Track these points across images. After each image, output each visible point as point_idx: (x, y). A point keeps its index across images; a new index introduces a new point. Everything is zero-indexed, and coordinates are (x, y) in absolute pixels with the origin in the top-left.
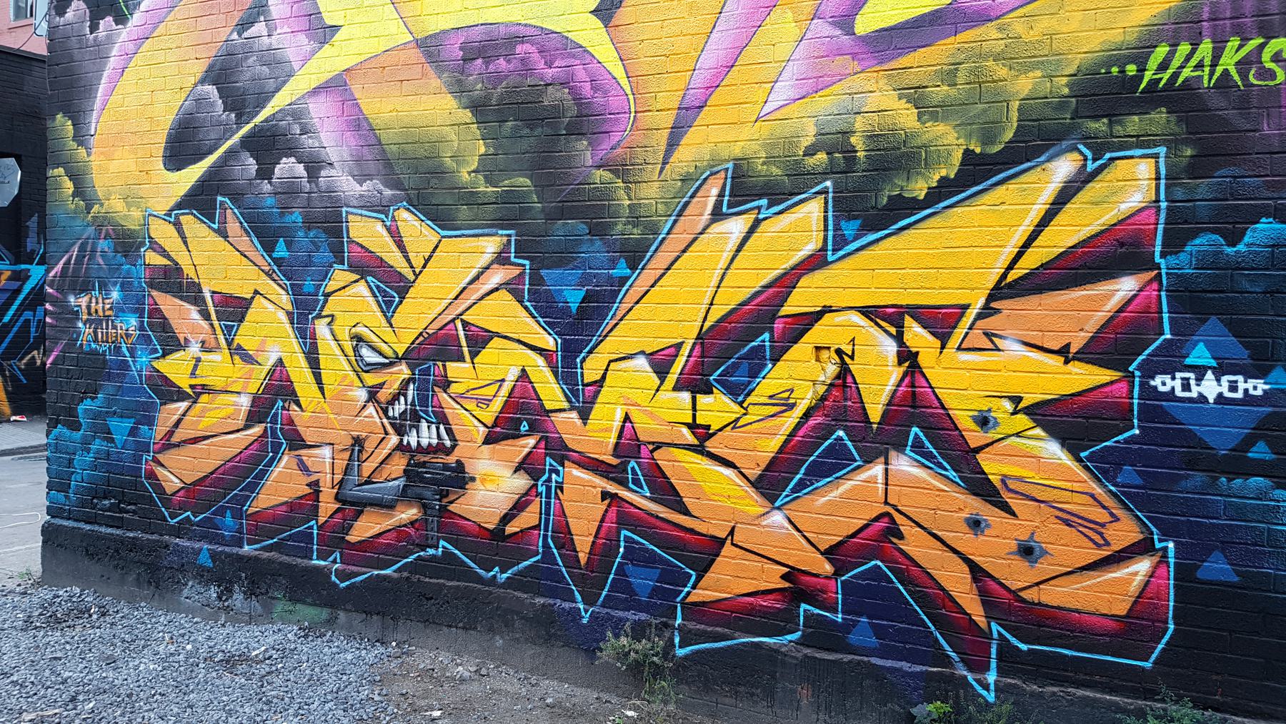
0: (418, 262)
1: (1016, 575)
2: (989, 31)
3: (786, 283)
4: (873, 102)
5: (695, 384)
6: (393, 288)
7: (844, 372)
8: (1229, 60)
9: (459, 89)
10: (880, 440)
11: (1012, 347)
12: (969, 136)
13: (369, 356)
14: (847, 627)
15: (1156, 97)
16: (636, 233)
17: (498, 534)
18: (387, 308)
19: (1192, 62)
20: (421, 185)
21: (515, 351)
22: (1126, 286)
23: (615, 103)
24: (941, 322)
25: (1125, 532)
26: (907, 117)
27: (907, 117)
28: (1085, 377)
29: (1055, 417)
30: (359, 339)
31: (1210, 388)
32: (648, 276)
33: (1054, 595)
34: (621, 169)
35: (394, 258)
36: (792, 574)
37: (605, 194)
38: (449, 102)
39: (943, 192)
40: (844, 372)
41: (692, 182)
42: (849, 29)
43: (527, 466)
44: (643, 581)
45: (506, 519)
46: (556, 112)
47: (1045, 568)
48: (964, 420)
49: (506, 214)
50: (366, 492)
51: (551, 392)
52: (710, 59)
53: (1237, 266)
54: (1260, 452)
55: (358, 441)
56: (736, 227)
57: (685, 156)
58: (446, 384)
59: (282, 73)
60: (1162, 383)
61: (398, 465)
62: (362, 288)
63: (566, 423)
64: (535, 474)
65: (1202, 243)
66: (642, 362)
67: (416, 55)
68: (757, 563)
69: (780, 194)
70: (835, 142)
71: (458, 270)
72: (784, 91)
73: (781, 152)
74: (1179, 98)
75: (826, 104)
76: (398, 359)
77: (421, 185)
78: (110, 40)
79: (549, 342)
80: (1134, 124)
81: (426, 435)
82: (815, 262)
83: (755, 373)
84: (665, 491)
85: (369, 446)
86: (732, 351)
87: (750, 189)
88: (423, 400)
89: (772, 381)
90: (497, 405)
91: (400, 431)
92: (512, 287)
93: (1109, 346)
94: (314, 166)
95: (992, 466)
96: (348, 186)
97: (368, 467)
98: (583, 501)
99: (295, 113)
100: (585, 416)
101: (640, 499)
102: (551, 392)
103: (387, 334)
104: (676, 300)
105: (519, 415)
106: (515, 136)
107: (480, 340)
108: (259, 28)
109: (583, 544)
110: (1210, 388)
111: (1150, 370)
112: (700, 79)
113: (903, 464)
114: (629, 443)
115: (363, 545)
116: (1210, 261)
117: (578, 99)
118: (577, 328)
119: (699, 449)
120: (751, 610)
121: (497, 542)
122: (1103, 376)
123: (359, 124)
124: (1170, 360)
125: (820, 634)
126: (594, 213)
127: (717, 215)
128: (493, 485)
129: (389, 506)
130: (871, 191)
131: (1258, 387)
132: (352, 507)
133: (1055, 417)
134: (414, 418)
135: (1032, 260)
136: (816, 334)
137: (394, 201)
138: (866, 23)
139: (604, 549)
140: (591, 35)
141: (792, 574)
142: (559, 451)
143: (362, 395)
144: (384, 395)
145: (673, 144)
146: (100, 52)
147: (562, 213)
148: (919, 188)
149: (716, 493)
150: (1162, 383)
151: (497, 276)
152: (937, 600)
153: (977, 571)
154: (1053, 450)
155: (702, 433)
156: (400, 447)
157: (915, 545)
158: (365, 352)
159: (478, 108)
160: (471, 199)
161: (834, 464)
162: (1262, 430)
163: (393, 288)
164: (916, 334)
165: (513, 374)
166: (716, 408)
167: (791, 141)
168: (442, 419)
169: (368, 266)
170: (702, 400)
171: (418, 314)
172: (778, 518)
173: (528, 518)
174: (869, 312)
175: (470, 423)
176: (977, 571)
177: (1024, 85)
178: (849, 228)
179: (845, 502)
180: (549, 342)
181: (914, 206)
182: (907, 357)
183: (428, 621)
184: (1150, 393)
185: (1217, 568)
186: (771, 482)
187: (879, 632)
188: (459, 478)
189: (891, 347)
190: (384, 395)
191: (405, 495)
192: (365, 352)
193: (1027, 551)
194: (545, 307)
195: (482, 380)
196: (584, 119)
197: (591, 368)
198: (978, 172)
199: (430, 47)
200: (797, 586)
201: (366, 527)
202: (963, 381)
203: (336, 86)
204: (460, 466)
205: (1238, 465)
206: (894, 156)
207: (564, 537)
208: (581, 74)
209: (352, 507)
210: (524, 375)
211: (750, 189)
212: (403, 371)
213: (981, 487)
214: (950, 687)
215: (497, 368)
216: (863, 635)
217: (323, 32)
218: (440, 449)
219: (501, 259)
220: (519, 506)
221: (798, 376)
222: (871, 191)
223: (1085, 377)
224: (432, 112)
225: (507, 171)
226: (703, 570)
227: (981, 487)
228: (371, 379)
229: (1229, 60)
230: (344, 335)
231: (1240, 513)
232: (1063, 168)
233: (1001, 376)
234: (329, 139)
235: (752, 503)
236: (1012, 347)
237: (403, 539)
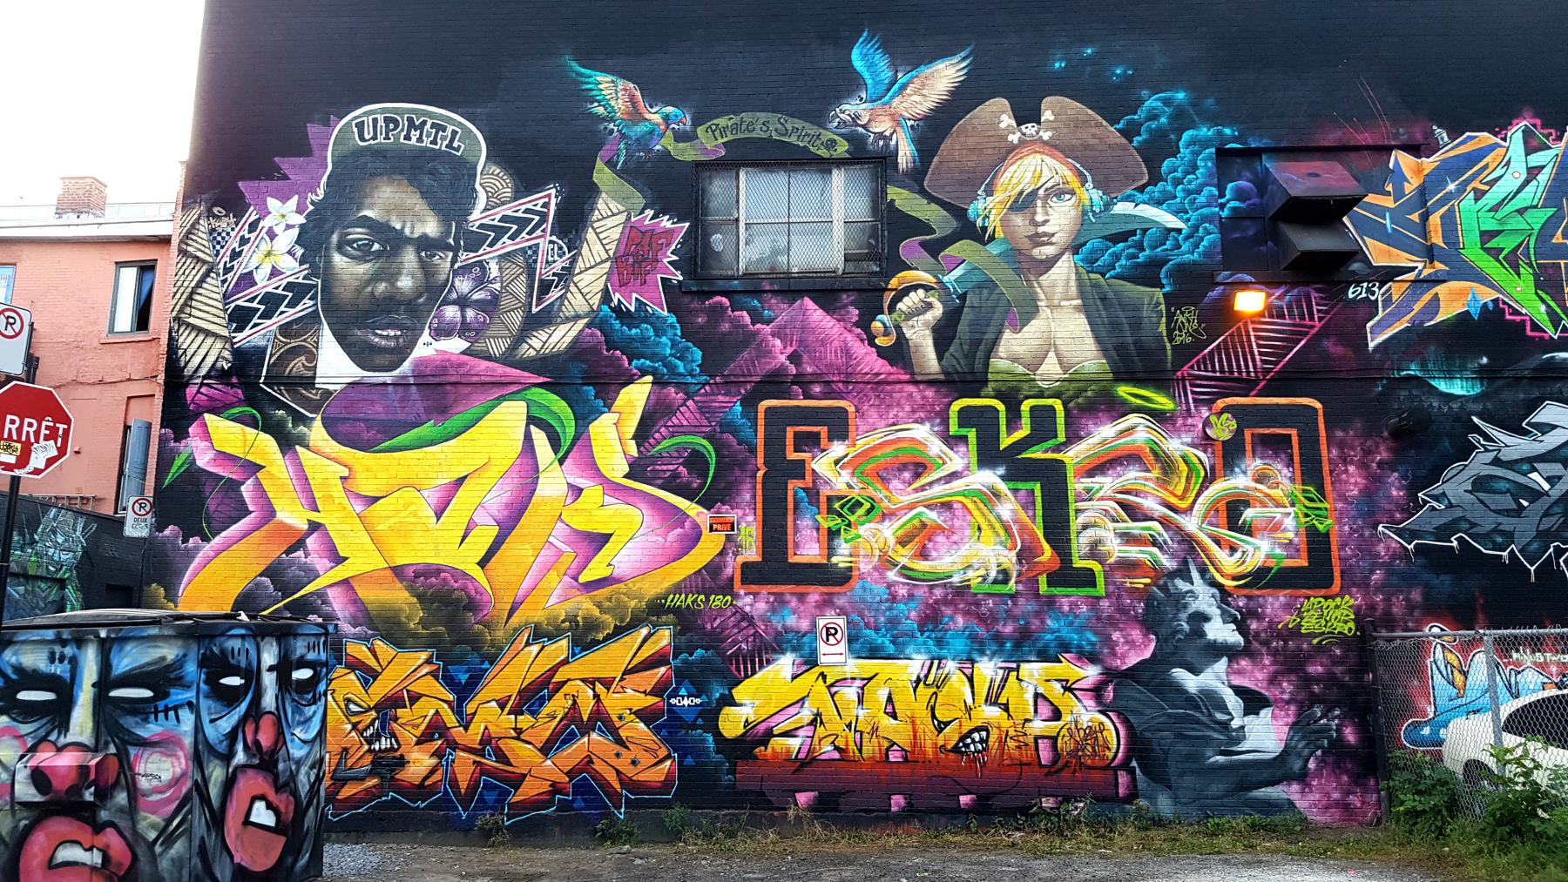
0: (384, 664)
1: (630, 771)
2: (622, 585)
3: (554, 669)
4: (585, 606)
5: (517, 711)
6: (369, 675)
7: (575, 702)
8: (689, 601)
9: (411, 589)
10: (586, 729)
11: (629, 691)
12: (1462, 369)
13: (353, 707)
14: (573, 801)
15: (671, 610)
16: (493, 651)
17: (421, 786)
18: (366, 684)
19: (679, 600)
20: (388, 628)
21: (435, 700)
22: (663, 670)
23: (485, 598)
24: (607, 683)
25: (663, 752)
26: (596, 612)
27: (596, 612)
28: (652, 700)
29: (644, 715)
30: (349, 700)
31: (686, 702)
32: (498, 668)
33: (642, 777)
34: (487, 625)
35: (372, 662)
36: (553, 784)
37: (481, 634)
38: (406, 594)
39: (608, 638)
40: (575, 702)
41: (517, 631)
42: (576, 579)
43: (438, 754)
44: (491, 797)
45: (425, 779)
46: (459, 600)
47: (640, 768)
48: (615, 719)
49: (432, 642)
50: (349, 773)
51: (450, 719)
52: (526, 585)
53: (692, 663)
54: (700, 722)
55: (346, 750)
56: (535, 649)
57: (515, 620)
58: (396, 719)
59: (313, 575)
60: (673, 701)
61: (369, 758)
62: (352, 676)
63: (458, 733)
64: (441, 757)
65: (682, 656)
66: (494, 704)
67: (389, 573)
68: (539, 782)
69: (552, 636)
70: (572, 619)
71: (404, 668)
72: (553, 600)
73: (552, 620)
74: (676, 611)
75: (569, 605)
76: (370, 709)
77: (388, 628)
78: (197, 549)
79: (451, 697)
80: (664, 618)
81: (385, 743)
82: (565, 662)
83: (541, 705)
84: (502, 757)
85: (351, 752)
86: (532, 697)
87: (541, 634)
88: (383, 727)
89: (547, 709)
90: (423, 727)
91: (370, 743)
92: (434, 674)
93: (658, 690)
94: (329, 617)
95: (623, 734)
96: (346, 628)
97: (350, 763)
98: (464, 767)
99: (321, 594)
100: (466, 729)
101: (490, 762)
102: (450, 719)
103: (365, 697)
104: (508, 678)
105: (435, 729)
106: (438, 609)
107: (415, 698)
108: (300, 553)
109: (463, 785)
110: (686, 702)
111: (669, 698)
112: (521, 592)
113: (594, 736)
114: (487, 739)
115: (347, 799)
116: (685, 662)
117: (469, 596)
118: (464, 692)
119: (518, 738)
120: (536, 802)
121: (421, 790)
122: (657, 699)
123: (356, 601)
124: (675, 694)
125: (564, 806)
126: (475, 643)
127: (528, 644)
128: (419, 763)
129: (363, 779)
130: (584, 637)
131: (698, 701)
132: (339, 781)
133: (644, 715)
134: (377, 736)
135: (635, 662)
136: (565, 689)
137: (373, 636)
138: (582, 579)
139: (473, 787)
140: (477, 573)
141: (553, 784)
142: (454, 746)
143: (349, 727)
144: (360, 727)
145: (510, 615)
146: (190, 555)
147: (459, 642)
148: (600, 637)
149: (524, 755)
150: (673, 701)
151: (426, 670)
152: (605, 786)
153: (618, 772)
154: (642, 725)
155: (519, 731)
156: (370, 751)
157: (598, 766)
158: (352, 706)
159: (421, 598)
160: (415, 635)
161: (571, 738)
162: (700, 714)
163: (369, 675)
164: (599, 688)
165: (432, 712)
166: (525, 720)
167: (556, 618)
168: (393, 735)
169: (355, 665)
170: (520, 718)
171: (380, 689)
172: (549, 762)
173: (437, 777)
174: (583, 680)
175: (408, 736)
176: (618, 772)
177: (633, 603)
178: (577, 650)
179: (572, 754)
180: (451, 697)
181: (599, 642)
182: (596, 696)
183: (382, 831)
184: (669, 704)
185: (689, 760)
186: (545, 750)
187: (585, 801)
188: (402, 762)
189: (591, 693)
190: (360, 727)
191: (371, 774)
192: (352, 706)
193: (634, 763)
194: (450, 682)
195: (412, 719)
196: (472, 605)
197: (470, 708)
198: (619, 632)
199: (398, 571)
200: (556, 788)
201: (348, 791)
202: (615, 703)
203: (345, 582)
204: (402, 756)
205: (694, 727)
206: (592, 625)
207: (454, 783)
208: (470, 586)
209: (339, 781)
210: (437, 712)
211: (541, 634)
212: (374, 714)
213: (620, 742)
214: (609, 815)
215: (426, 710)
216: (579, 804)
217: (339, 560)
218: (392, 749)
219: (428, 662)
220: (432, 772)
221: (557, 706)
222: (584, 637)
223: (652, 700)
224: (399, 597)
225: (433, 624)
226: (517, 788)
227: (620, 742)
228: (354, 719)
229: (689, 601)
230: (340, 698)
231: (695, 742)
232: (644, 631)
233: (626, 701)
234: (338, 604)
235: (539, 758)
236: (629, 691)
237: (369, 794)
